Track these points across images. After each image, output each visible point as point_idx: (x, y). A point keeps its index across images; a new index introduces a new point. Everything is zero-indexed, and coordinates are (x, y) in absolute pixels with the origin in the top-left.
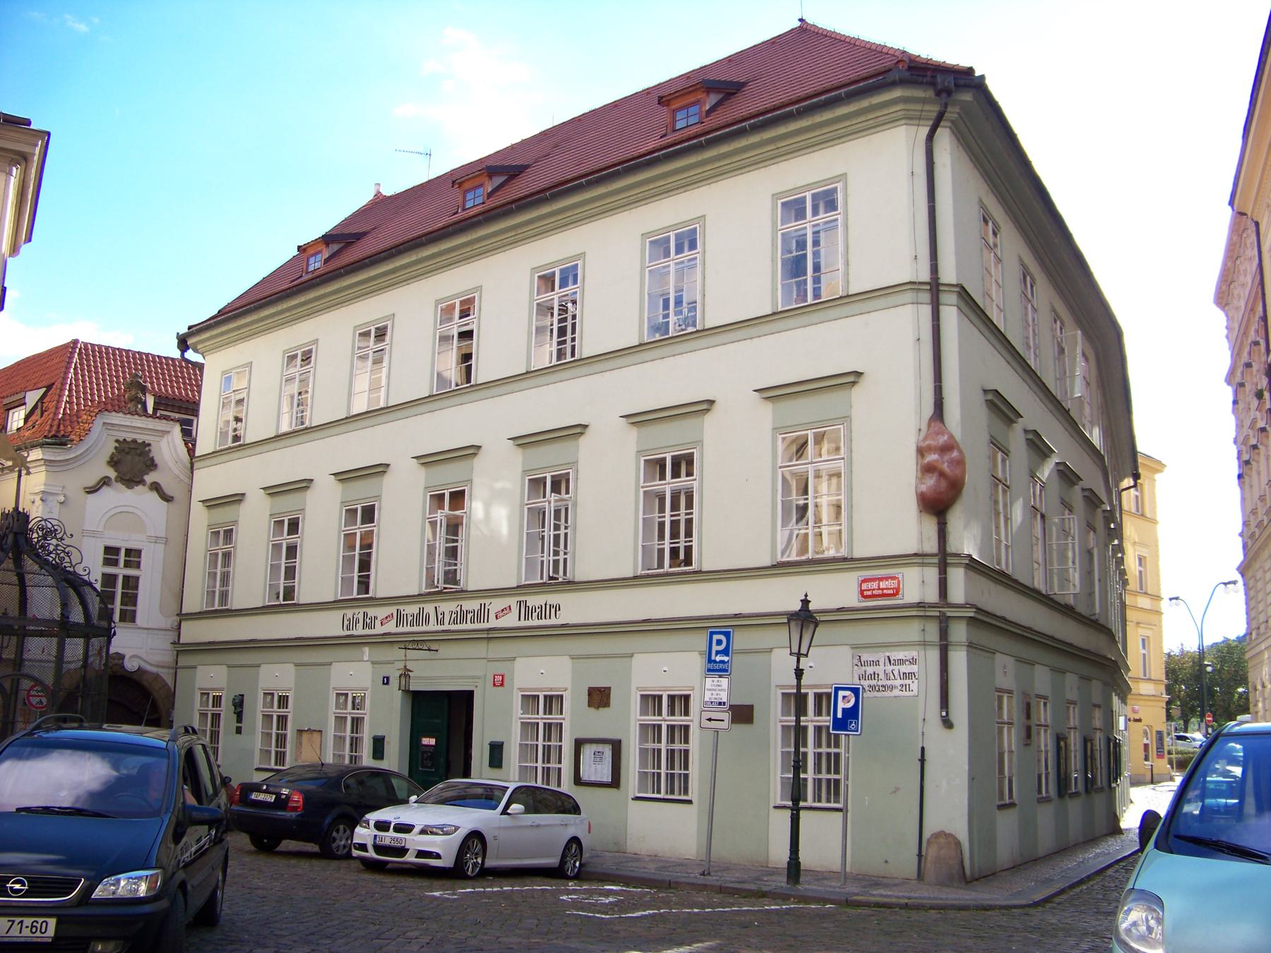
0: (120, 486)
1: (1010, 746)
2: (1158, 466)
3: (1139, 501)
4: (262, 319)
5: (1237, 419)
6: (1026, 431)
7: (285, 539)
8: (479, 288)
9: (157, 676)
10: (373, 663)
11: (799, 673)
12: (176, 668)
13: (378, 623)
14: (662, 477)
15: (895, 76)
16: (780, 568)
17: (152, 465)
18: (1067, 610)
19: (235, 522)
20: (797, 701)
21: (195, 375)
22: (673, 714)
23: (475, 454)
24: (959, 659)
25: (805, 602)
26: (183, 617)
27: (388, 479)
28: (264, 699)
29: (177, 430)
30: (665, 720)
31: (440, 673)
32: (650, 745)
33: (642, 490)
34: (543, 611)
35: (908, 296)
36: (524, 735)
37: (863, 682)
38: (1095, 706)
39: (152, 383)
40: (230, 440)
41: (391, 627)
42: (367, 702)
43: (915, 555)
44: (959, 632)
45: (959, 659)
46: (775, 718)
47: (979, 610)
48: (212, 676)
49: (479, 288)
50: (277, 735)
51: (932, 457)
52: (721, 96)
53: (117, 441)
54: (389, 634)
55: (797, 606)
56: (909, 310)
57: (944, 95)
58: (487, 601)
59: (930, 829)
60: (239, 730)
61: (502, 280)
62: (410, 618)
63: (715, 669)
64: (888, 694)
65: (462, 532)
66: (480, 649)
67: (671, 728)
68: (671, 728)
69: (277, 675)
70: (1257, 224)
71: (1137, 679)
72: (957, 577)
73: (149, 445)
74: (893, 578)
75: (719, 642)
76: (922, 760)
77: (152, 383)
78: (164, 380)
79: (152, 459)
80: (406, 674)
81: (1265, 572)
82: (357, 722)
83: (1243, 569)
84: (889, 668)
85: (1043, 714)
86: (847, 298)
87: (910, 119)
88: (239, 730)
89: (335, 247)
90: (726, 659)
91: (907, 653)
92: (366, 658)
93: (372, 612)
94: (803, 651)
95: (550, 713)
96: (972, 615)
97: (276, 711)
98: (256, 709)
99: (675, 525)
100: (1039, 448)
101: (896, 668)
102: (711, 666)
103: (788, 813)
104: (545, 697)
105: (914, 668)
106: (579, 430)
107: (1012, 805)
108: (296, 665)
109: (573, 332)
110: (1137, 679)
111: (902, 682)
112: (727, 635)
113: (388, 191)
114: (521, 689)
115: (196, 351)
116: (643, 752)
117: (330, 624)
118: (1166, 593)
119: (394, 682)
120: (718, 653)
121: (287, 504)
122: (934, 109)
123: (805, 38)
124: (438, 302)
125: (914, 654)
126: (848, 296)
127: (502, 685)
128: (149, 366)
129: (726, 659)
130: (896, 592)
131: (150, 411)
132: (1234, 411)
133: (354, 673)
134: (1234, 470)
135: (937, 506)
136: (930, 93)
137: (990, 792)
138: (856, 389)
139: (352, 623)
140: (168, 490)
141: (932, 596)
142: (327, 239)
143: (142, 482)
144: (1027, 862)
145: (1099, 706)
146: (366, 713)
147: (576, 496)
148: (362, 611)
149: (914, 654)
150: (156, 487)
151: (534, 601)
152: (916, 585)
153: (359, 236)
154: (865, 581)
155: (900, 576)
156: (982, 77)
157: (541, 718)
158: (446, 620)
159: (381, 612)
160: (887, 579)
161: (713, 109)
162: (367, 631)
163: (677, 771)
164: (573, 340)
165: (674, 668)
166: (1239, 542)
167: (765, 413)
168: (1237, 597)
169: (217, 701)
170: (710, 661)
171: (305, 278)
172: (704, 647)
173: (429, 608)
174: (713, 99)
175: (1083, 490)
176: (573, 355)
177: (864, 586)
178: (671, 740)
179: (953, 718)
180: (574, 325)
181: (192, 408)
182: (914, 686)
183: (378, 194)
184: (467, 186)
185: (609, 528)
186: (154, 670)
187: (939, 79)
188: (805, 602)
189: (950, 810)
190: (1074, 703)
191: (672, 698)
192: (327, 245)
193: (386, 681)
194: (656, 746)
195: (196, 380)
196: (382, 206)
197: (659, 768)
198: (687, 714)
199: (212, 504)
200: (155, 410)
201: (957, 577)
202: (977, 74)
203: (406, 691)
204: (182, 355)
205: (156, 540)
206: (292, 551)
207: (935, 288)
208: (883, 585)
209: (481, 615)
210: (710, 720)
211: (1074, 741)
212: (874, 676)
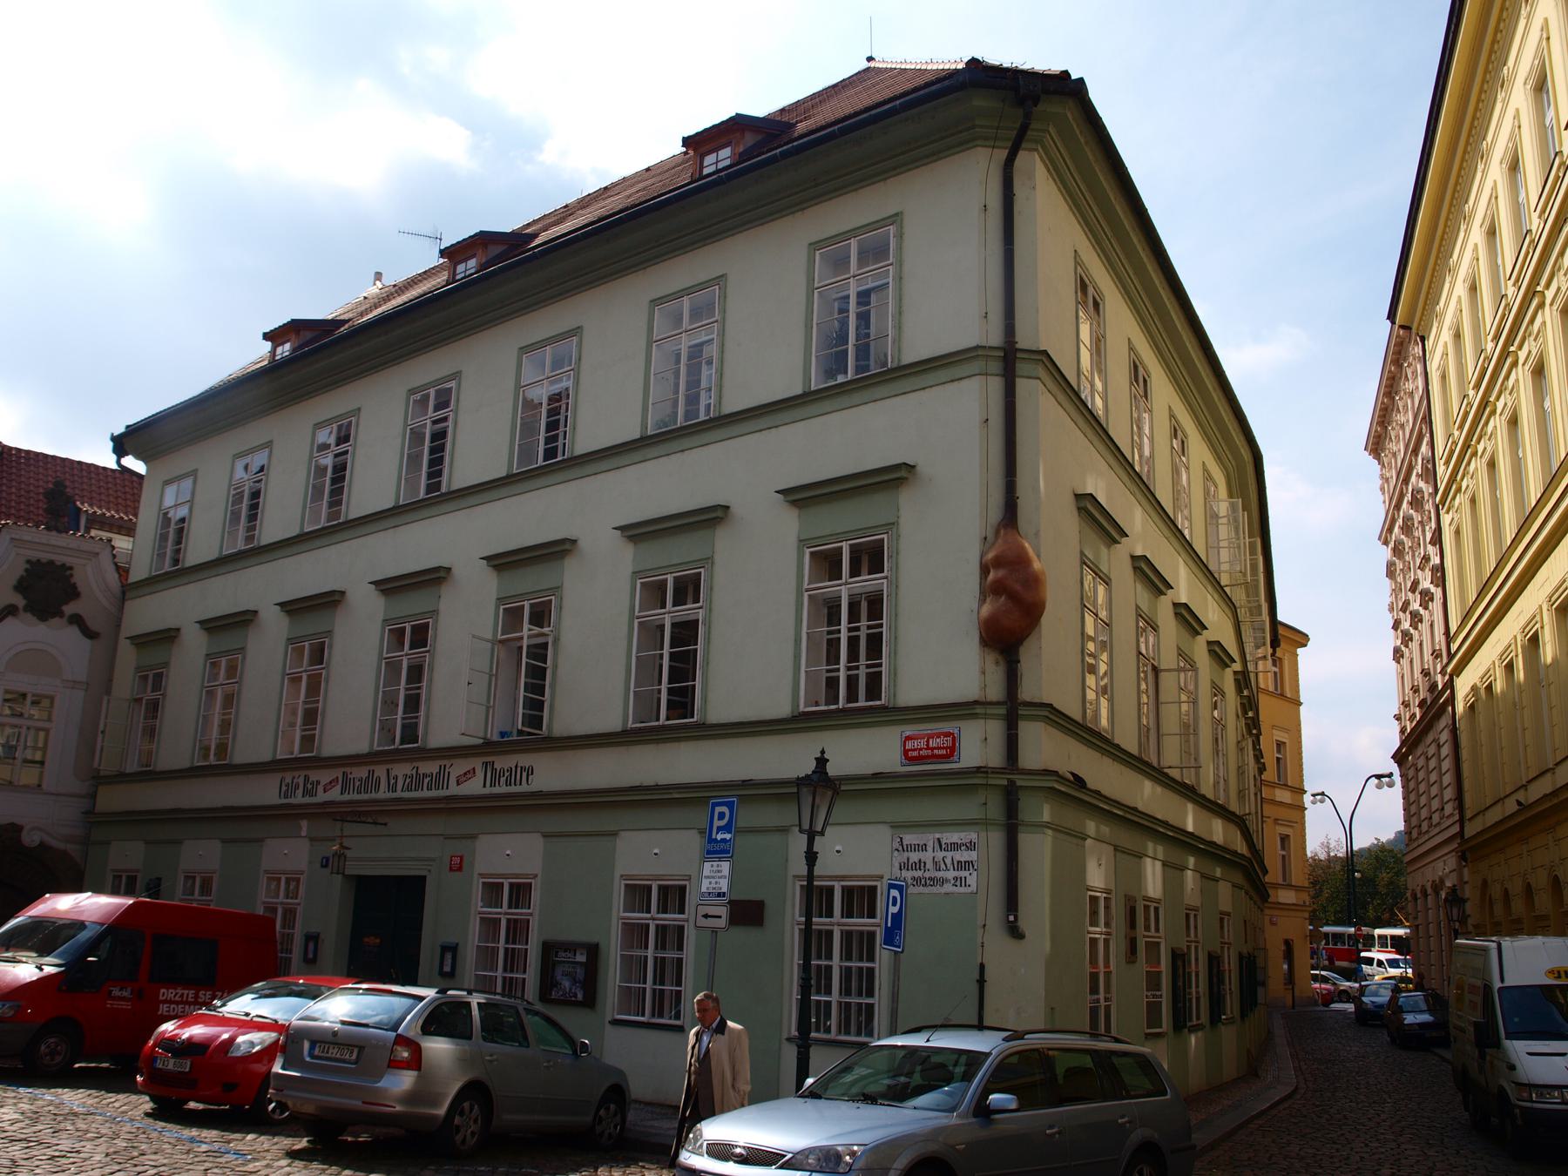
0: (29, 615)
3: (1278, 678)
7: (669, 615)
10: (312, 840)
11: (811, 857)
13: (320, 789)
16: (798, 723)
17: (73, 593)
20: (816, 897)
25: (822, 762)
30: (654, 918)
31: (378, 854)
34: (512, 776)
37: (905, 873)
41: (335, 794)
42: (536, 895)
46: (789, 916)
52: (759, 137)
53: (28, 562)
55: (808, 767)
56: (974, 385)
58: (447, 762)
63: (715, 851)
67: (662, 930)
71: (1276, 886)
73: (71, 568)
74: (947, 735)
76: (981, 982)
79: (74, 586)
83: (1399, 757)
84: (940, 855)
90: (728, 836)
91: (963, 835)
93: (314, 776)
97: (503, 912)
99: (853, 642)
100: (1150, 576)
101: (949, 854)
102: (710, 847)
104: (660, 887)
108: (224, 841)
110: (1276, 886)
111: (956, 874)
112: (730, 805)
117: (265, 792)
118: (1311, 786)
120: (719, 829)
125: (973, 836)
127: (460, 869)
129: (728, 836)
130: (951, 752)
133: (291, 853)
140: (93, 625)
141: (995, 758)
143: (61, 614)
146: (534, 913)
148: (303, 773)
149: (973, 836)
150: (77, 620)
154: (908, 738)
156: (1081, 81)
157: (654, 918)
159: (324, 776)
162: (308, 800)
172: (705, 825)
173: (380, 771)
177: (909, 745)
179: (1023, 924)
182: (972, 880)
186: (60, 845)
188: (822, 762)
191: (663, 890)
194: (640, 953)
198: (682, 911)
199: (144, 641)
202: (1074, 77)
204: (118, 462)
210: (706, 916)
212: (920, 865)
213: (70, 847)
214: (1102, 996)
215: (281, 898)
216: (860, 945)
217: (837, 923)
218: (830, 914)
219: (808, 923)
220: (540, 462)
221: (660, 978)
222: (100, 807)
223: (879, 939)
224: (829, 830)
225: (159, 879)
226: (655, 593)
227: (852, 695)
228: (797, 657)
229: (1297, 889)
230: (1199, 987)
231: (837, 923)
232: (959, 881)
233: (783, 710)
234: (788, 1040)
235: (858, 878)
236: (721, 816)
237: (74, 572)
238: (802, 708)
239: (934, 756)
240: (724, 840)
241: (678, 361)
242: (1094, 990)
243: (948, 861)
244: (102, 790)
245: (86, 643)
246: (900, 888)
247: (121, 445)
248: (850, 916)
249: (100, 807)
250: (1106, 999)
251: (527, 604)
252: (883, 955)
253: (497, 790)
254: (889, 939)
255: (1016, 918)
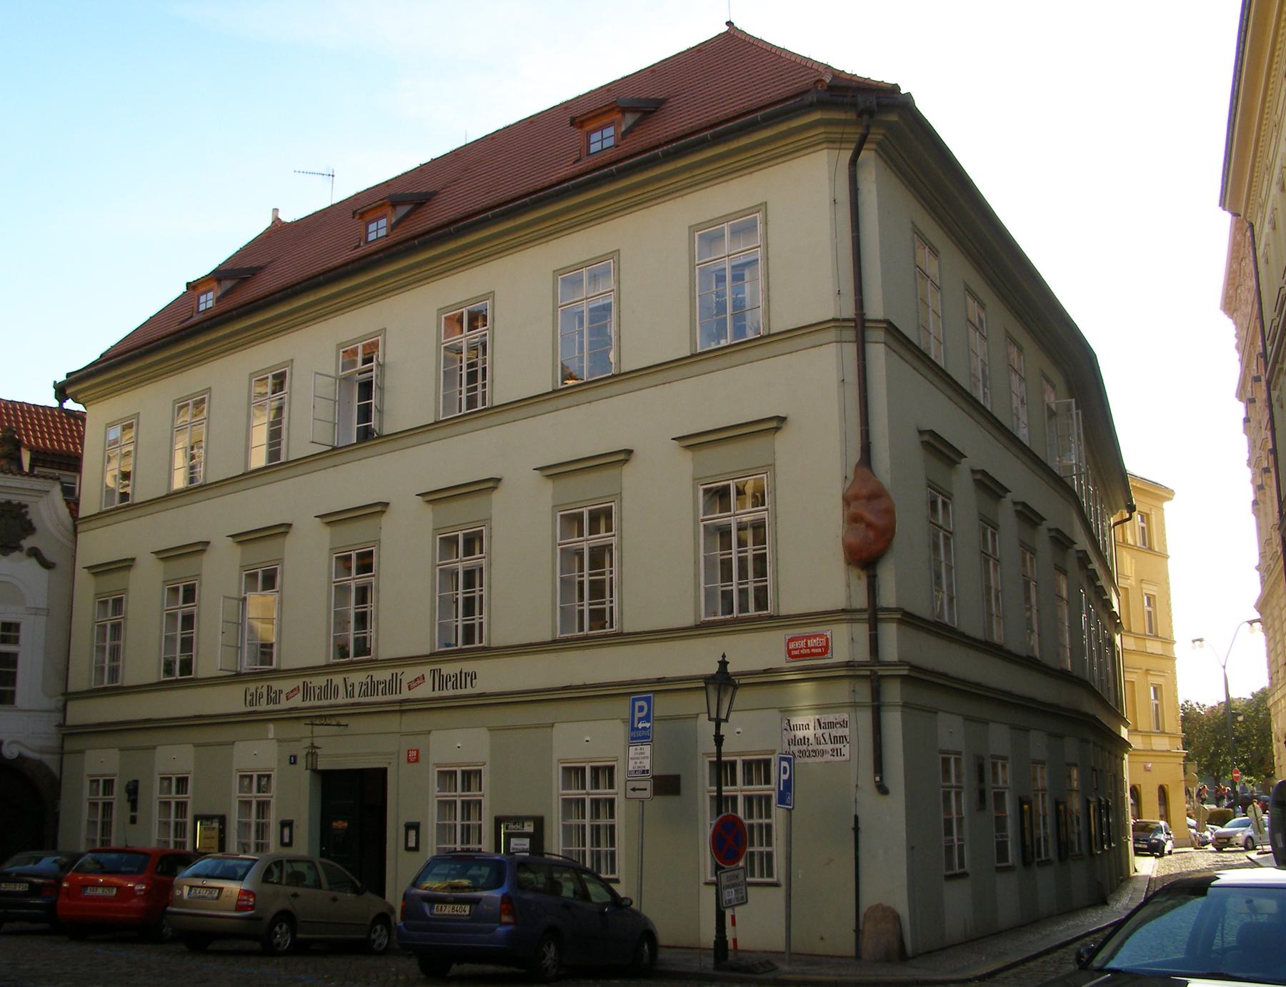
1: (959, 812)
2: (1160, 493)
4: (150, 366)
5: (1249, 439)
6: (973, 471)
7: (181, 609)
8: (383, 331)
9: (40, 764)
10: (279, 741)
11: (719, 740)
12: (62, 752)
13: (283, 697)
14: (581, 534)
15: (811, 98)
16: (701, 629)
17: (29, 529)
18: (1030, 663)
19: (125, 591)
20: (722, 770)
21: (77, 426)
22: (597, 787)
23: (383, 512)
24: (893, 721)
25: (723, 664)
26: (69, 697)
27: (289, 541)
28: (161, 784)
29: (57, 492)
30: (589, 793)
31: (349, 750)
32: (575, 821)
33: (559, 548)
34: (460, 680)
35: (832, 335)
36: (441, 815)
38: (1036, 762)
39: (28, 436)
40: (117, 498)
41: (297, 701)
42: (274, 782)
43: (844, 611)
44: (893, 692)
45: (893, 721)
47: (913, 667)
48: (103, 760)
49: (383, 331)
50: (258, 824)
51: (857, 508)
52: (638, 116)
54: (296, 709)
55: (713, 669)
57: (865, 117)
58: (399, 671)
59: (867, 901)
60: (133, 820)
61: (406, 324)
62: (317, 691)
63: (637, 737)
64: (818, 759)
65: (372, 595)
66: (392, 723)
67: (596, 803)
68: (596, 803)
69: (176, 756)
70: (1252, 226)
72: (890, 633)
73: (26, 506)
74: (821, 636)
75: (641, 709)
76: (856, 829)
77: (28, 436)
78: (42, 432)
79: (30, 523)
80: (313, 753)
81: (1281, 610)
82: (263, 806)
83: (1262, 605)
85: (1005, 777)
86: (768, 338)
87: (831, 142)
88: (133, 820)
89: (228, 284)
90: (648, 725)
92: (271, 736)
93: (276, 685)
94: (723, 716)
95: (469, 790)
96: (905, 673)
97: (174, 797)
98: (153, 795)
103: (713, 889)
105: (846, 732)
106: (492, 484)
107: (963, 875)
109: (484, 378)
111: (833, 746)
112: (648, 700)
113: (288, 216)
114: (437, 765)
115: (76, 401)
116: (567, 829)
117: (231, 700)
119: (302, 762)
120: (640, 719)
121: (182, 569)
122: (855, 132)
123: (733, 47)
124: (340, 346)
125: (845, 716)
126: (769, 336)
127: (417, 760)
128: (24, 417)
129: (648, 725)
130: (825, 650)
131: (26, 468)
132: (1246, 431)
133: (259, 752)
134: (1250, 496)
135: (865, 559)
136: (851, 116)
137: (934, 858)
138: (778, 435)
139: (256, 698)
140: (49, 555)
141: (863, 654)
142: (218, 275)
143: (18, 548)
144: (984, 935)
145: (1076, 765)
146: (273, 795)
147: (490, 554)
148: (266, 684)
150: (35, 553)
151: (449, 669)
152: (845, 643)
153: (254, 272)
154: (791, 640)
155: (828, 634)
157: (459, 795)
158: (356, 694)
159: (286, 685)
160: (815, 637)
161: (629, 131)
162: (272, 707)
163: (603, 848)
164: (484, 386)
165: (595, 737)
166: (1256, 576)
167: (685, 463)
168: (1257, 641)
169: (109, 784)
170: (633, 729)
171: (196, 318)
172: (627, 715)
173: (338, 679)
174: (630, 119)
175: (1050, 530)
176: (484, 404)
177: (792, 646)
178: (596, 814)
180: (484, 369)
181: (72, 462)
182: (846, 750)
183: (276, 221)
184: (368, 217)
185: (523, 592)
187: (860, 98)
188: (723, 664)
189: (889, 884)
190: (1043, 763)
191: (595, 770)
192: (219, 281)
193: (293, 760)
194: (580, 821)
195: (79, 432)
196: (280, 235)
197: (584, 845)
198: (611, 786)
199: (99, 570)
200: (32, 466)
201: (890, 633)
202: (903, 92)
203: (315, 771)
204: (61, 405)
205: (36, 611)
206: (188, 621)
207: (858, 326)
208: (811, 643)
209: (393, 685)
210: (634, 789)
211: (1043, 806)
213: (46, 758)
214: (955, 837)
215: (101, 795)
216: (759, 804)
217: (739, 789)
218: (734, 783)
219: (719, 790)
220: (464, 411)
221: (596, 841)
222: (69, 722)
223: (774, 801)
224: (732, 715)
225: (136, 782)
226: (572, 521)
227: (744, 608)
228: (697, 576)
229: (1171, 736)
230: (1045, 830)
231: (739, 789)
232: (837, 752)
233: (689, 621)
234: (706, 884)
235: (329, 622)
236: (641, 709)
237: (31, 509)
238: (703, 618)
239: (812, 655)
240: (644, 728)
241: (581, 323)
242: (949, 832)
243: (827, 737)
244: (71, 705)
245: (45, 572)
246: (788, 760)
247: (61, 391)
248: (750, 783)
249: (69, 722)
250: (959, 840)
251: (260, 571)
252: (778, 813)
253: (445, 693)
254: (782, 800)
255: (881, 778)
